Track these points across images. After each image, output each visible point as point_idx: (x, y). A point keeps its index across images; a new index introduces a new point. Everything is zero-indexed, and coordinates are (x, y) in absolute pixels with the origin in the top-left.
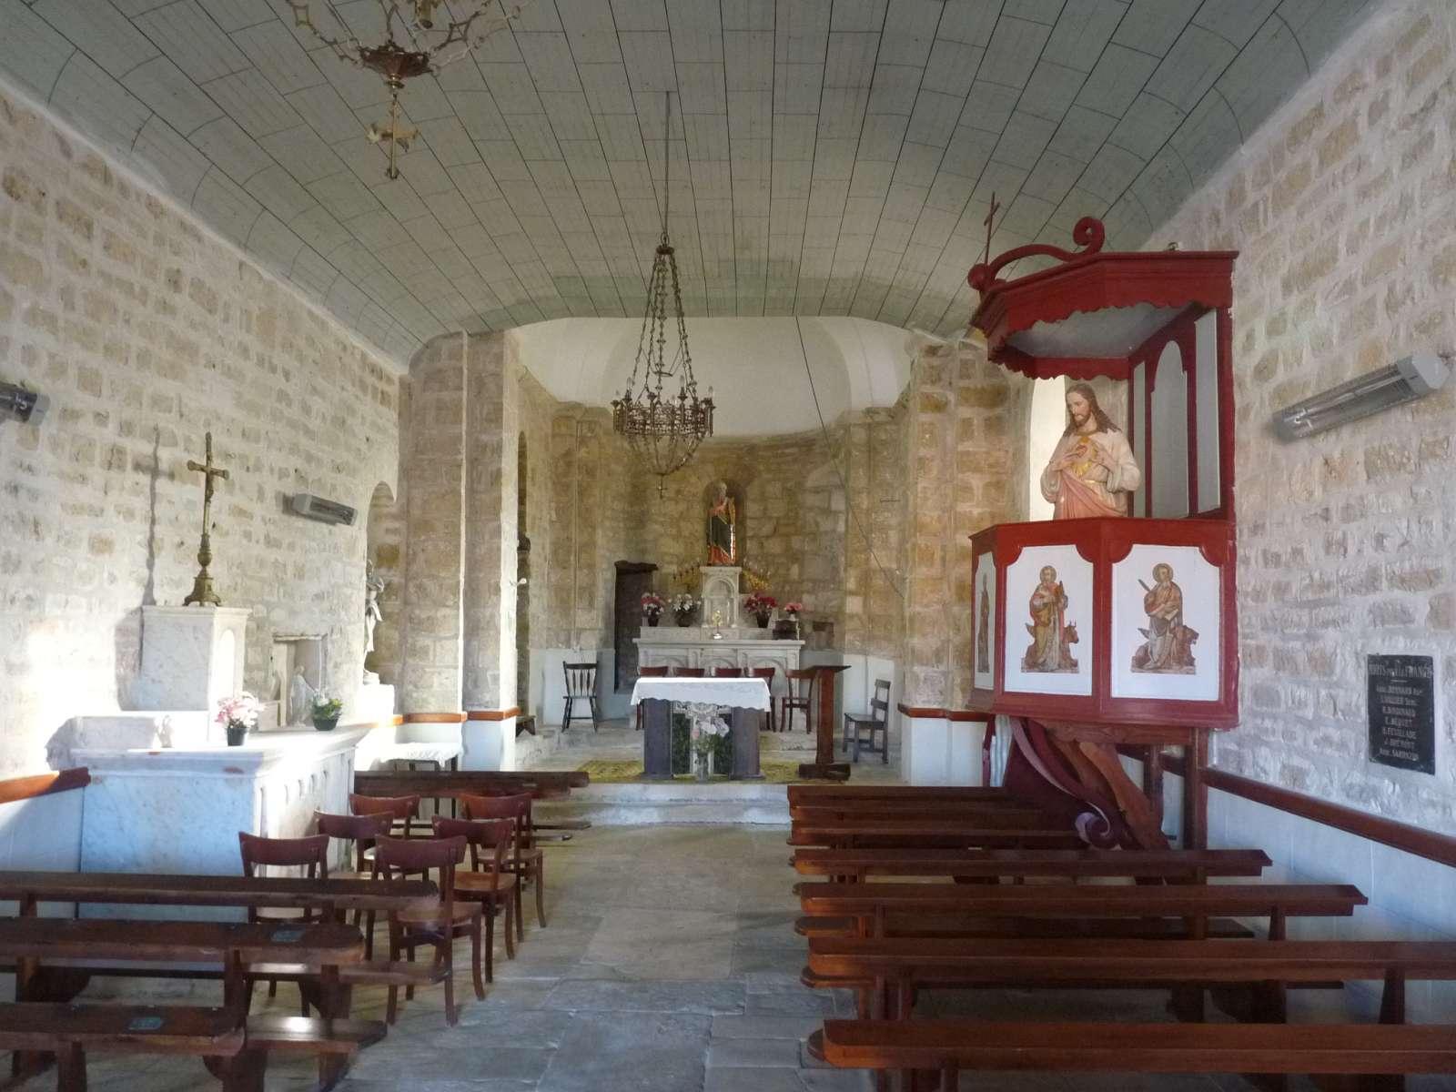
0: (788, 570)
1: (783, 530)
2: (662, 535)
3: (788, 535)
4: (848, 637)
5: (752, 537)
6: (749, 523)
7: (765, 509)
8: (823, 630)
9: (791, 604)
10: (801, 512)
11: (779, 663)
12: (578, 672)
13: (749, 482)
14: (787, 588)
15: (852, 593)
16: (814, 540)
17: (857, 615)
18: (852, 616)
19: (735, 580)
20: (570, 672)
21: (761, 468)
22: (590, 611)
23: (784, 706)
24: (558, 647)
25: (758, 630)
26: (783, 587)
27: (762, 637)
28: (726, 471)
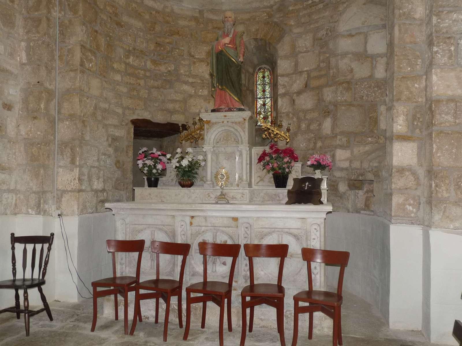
0: (320, 125)
1: (314, 83)
2: (191, 96)
3: (319, 88)
4: (397, 200)
5: (284, 95)
6: (281, 81)
7: (296, 65)
8: (359, 188)
9: (317, 156)
10: (333, 61)
11: (295, 236)
12: (30, 247)
13: (281, 38)
14: (319, 144)
15: (403, 138)
16: (348, 89)
17: (409, 169)
18: (401, 170)
19: (243, 129)
20: (19, 247)
21: (292, 23)
22: (72, 170)
23: (298, 310)
24: (28, 213)
25: (273, 190)
26: (315, 143)
27: (274, 200)
28: (257, 30)
